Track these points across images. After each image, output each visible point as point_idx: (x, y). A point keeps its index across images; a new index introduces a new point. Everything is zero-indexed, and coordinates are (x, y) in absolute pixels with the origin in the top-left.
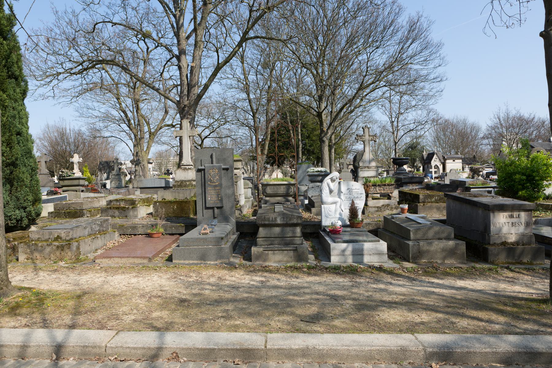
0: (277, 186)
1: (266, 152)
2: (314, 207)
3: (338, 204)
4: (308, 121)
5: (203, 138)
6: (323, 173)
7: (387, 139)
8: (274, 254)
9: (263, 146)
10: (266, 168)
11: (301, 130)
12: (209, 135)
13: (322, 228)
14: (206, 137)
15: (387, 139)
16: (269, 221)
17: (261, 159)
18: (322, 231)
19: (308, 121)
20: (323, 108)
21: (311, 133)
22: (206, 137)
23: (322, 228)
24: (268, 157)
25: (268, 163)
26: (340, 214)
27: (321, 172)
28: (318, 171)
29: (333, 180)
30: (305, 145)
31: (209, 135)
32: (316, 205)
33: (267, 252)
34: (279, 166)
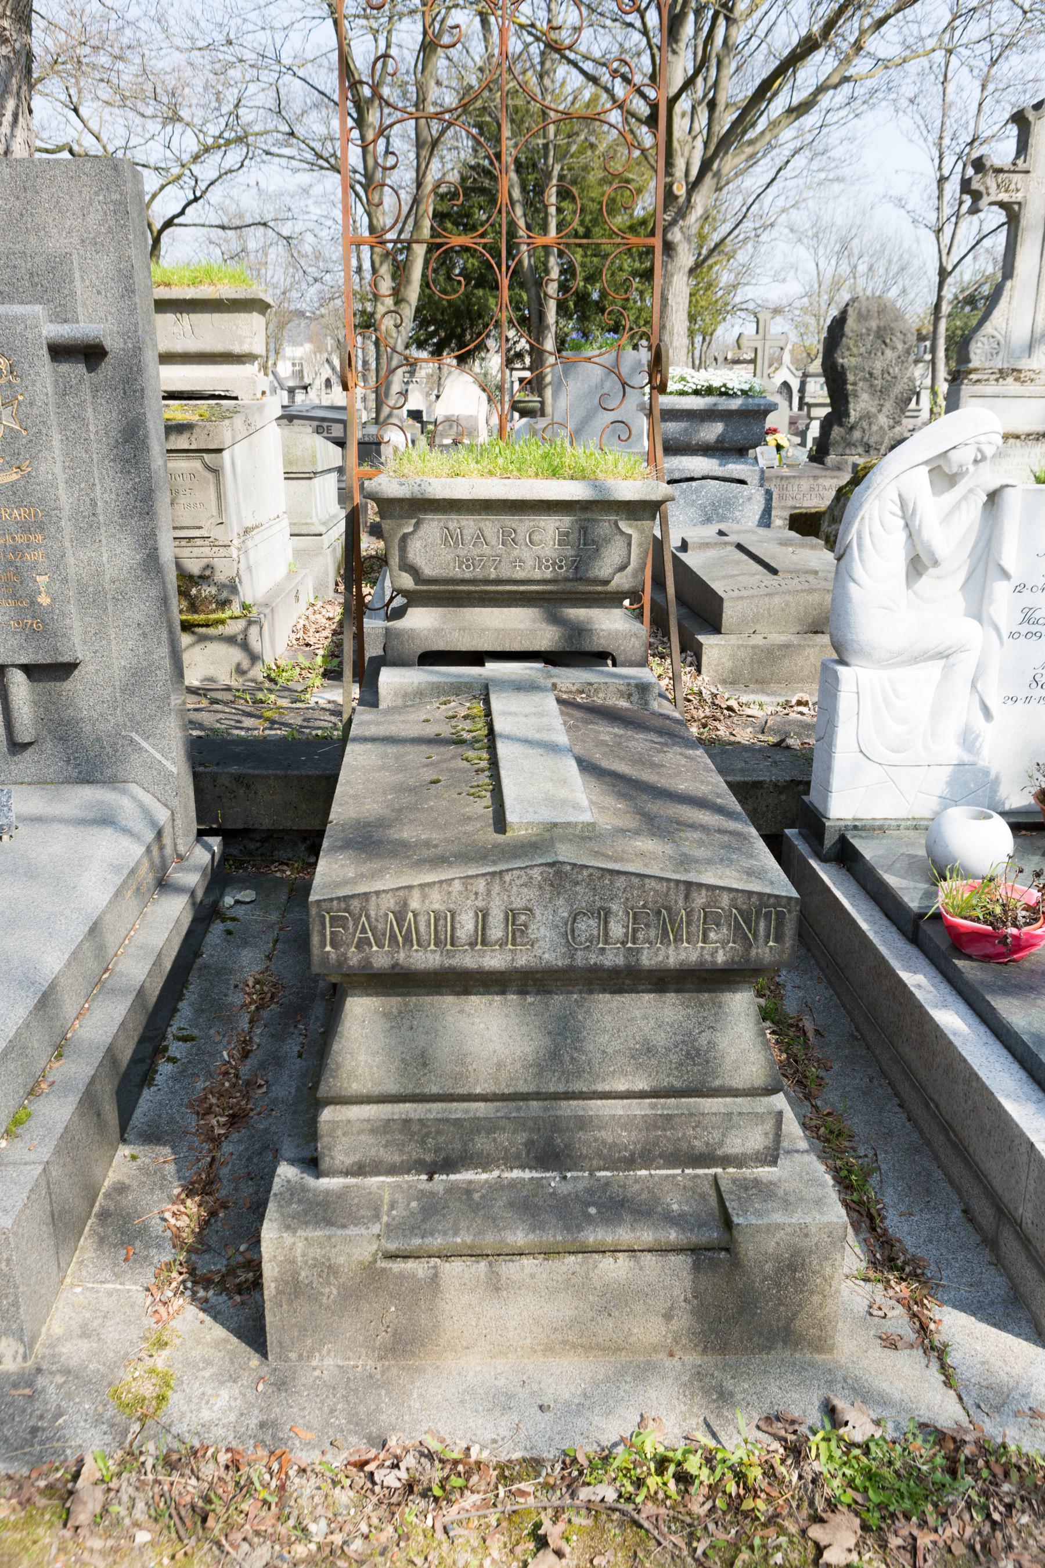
0: (510, 521)
1: (413, 293)
2: (715, 627)
3: (966, 665)
4: (585, 168)
5: (157, 225)
6: (735, 404)
7: (862, 268)
8: (495, 1286)
9: (400, 272)
10: (412, 365)
11: (559, 210)
12: (182, 212)
13: (829, 840)
14: (169, 224)
15: (862, 268)
16: (446, 940)
17: (398, 326)
18: (823, 859)
19: (585, 168)
20: (678, 82)
21: (595, 222)
22: (169, 224)
23: (829, 840)
24: (422, 319)
25: (421, 345)
26: (968, 740)
27: (725, 393)
28: (709, 391)
29: (943, 474)
30: (568, 271)
31: (182, 212)
32: (730, 614)
33: (417, 1268)
34: (462, 360)
